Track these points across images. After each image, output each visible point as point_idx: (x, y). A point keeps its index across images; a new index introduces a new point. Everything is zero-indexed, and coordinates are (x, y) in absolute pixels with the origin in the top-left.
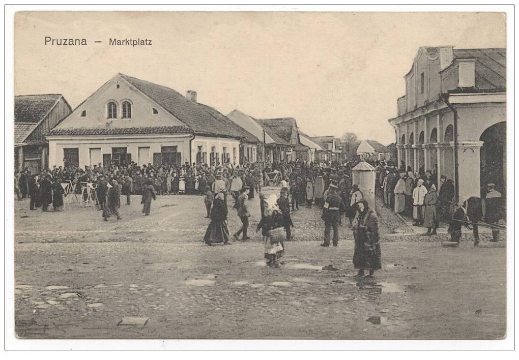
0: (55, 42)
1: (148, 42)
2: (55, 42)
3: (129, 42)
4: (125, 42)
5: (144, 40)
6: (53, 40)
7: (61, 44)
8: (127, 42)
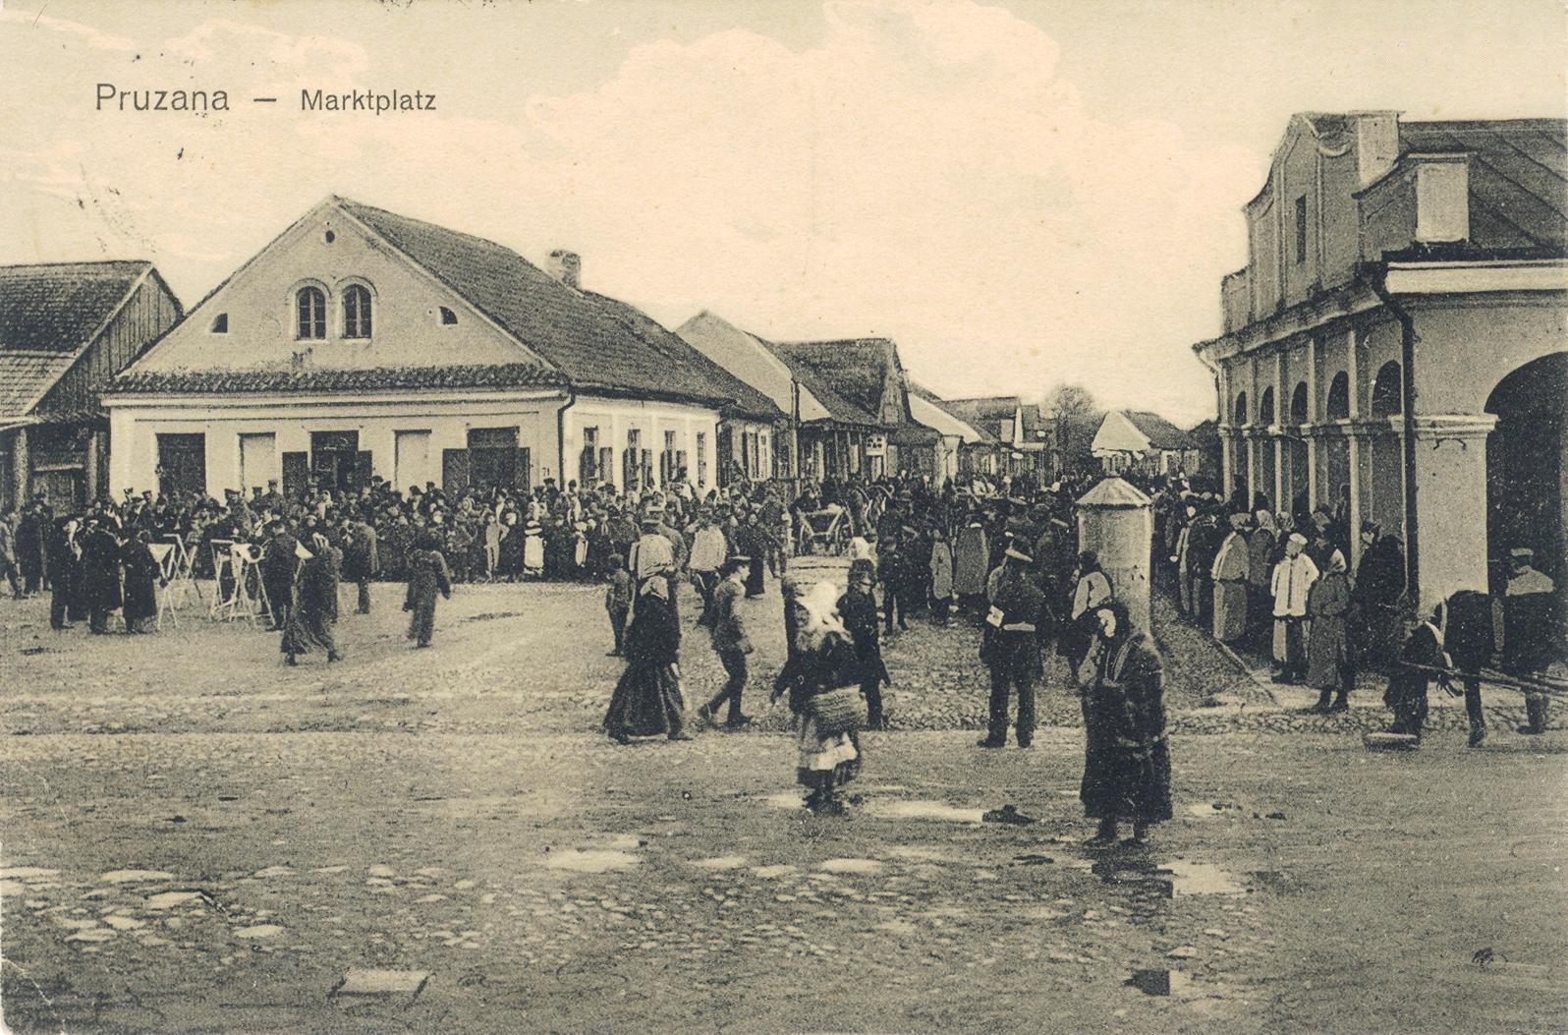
0: (129, 101)
1: (424, 102)
2: (129, 101)
3: (365, 101)
4: (349, 102)
5: (413, 94)
6: (122, 95)
7: (147, 106)
8: (358, 100)
